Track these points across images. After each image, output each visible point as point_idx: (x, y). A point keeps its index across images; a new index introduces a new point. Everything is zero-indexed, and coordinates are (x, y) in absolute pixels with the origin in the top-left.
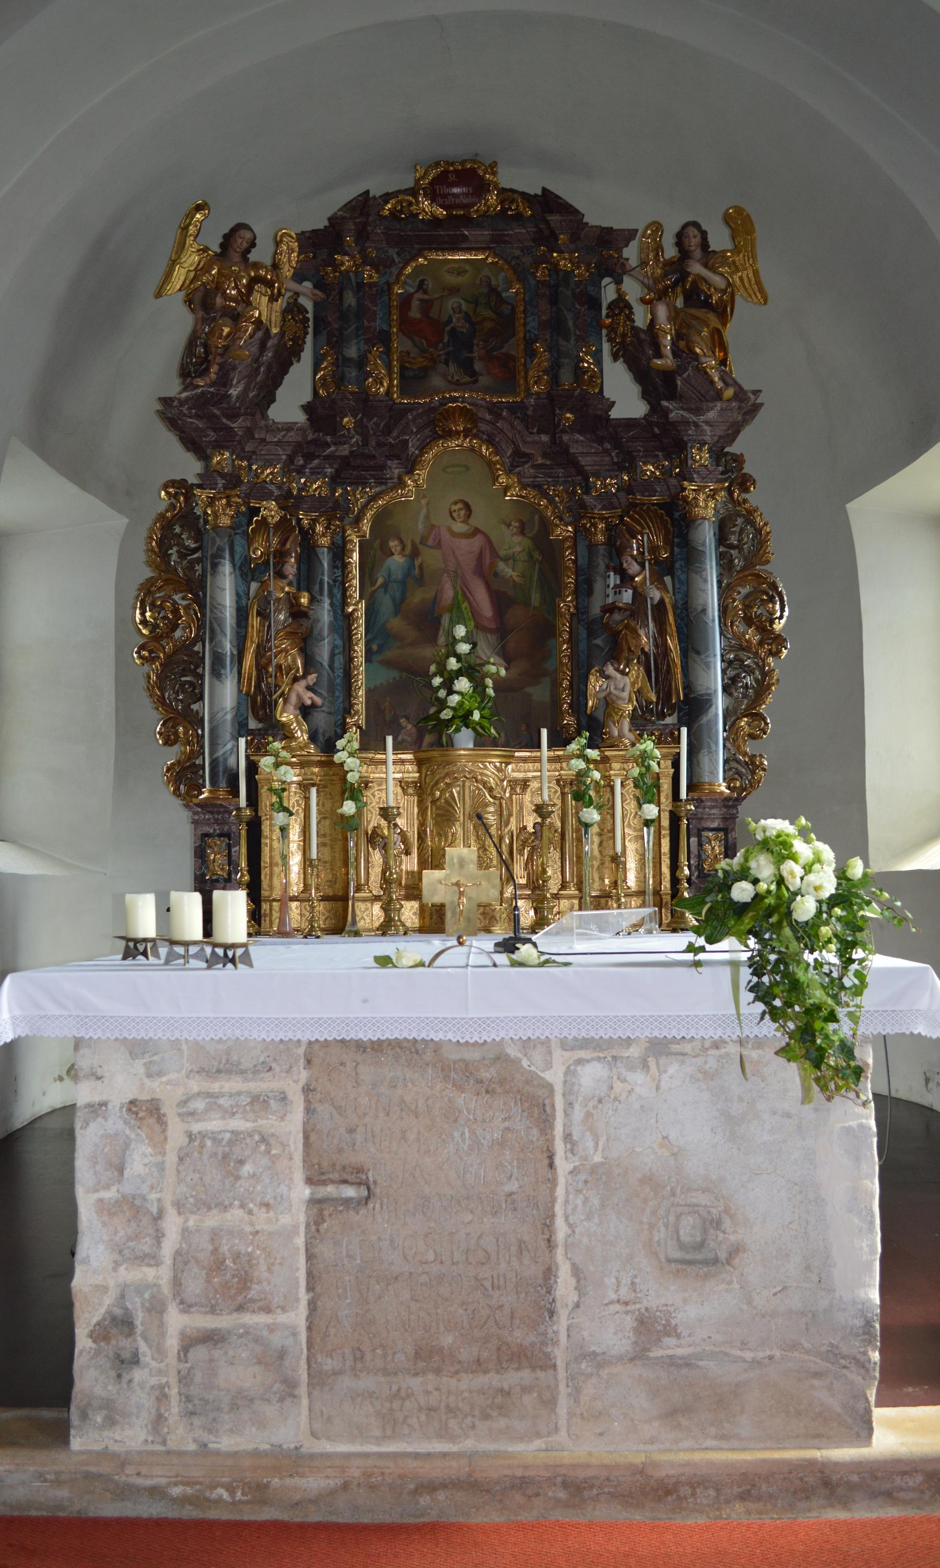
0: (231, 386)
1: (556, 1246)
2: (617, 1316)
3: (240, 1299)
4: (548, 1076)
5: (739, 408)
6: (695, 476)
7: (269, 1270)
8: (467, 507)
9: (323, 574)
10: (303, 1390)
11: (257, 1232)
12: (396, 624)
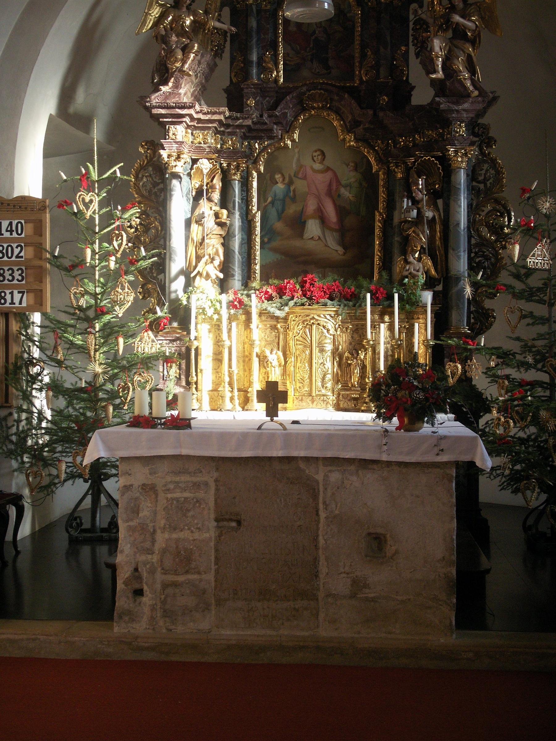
0: (181, 88)
1: (319, 549)
2: (344, 579)
3: (187, 568)
4: (316, 477)
5: (483, 101)
6: (456, 142)
7: (200, 556)
8: (323, 154)
9: (235, 197)
10: (213, 607)
11: (195, 540)
12: (279, 226)
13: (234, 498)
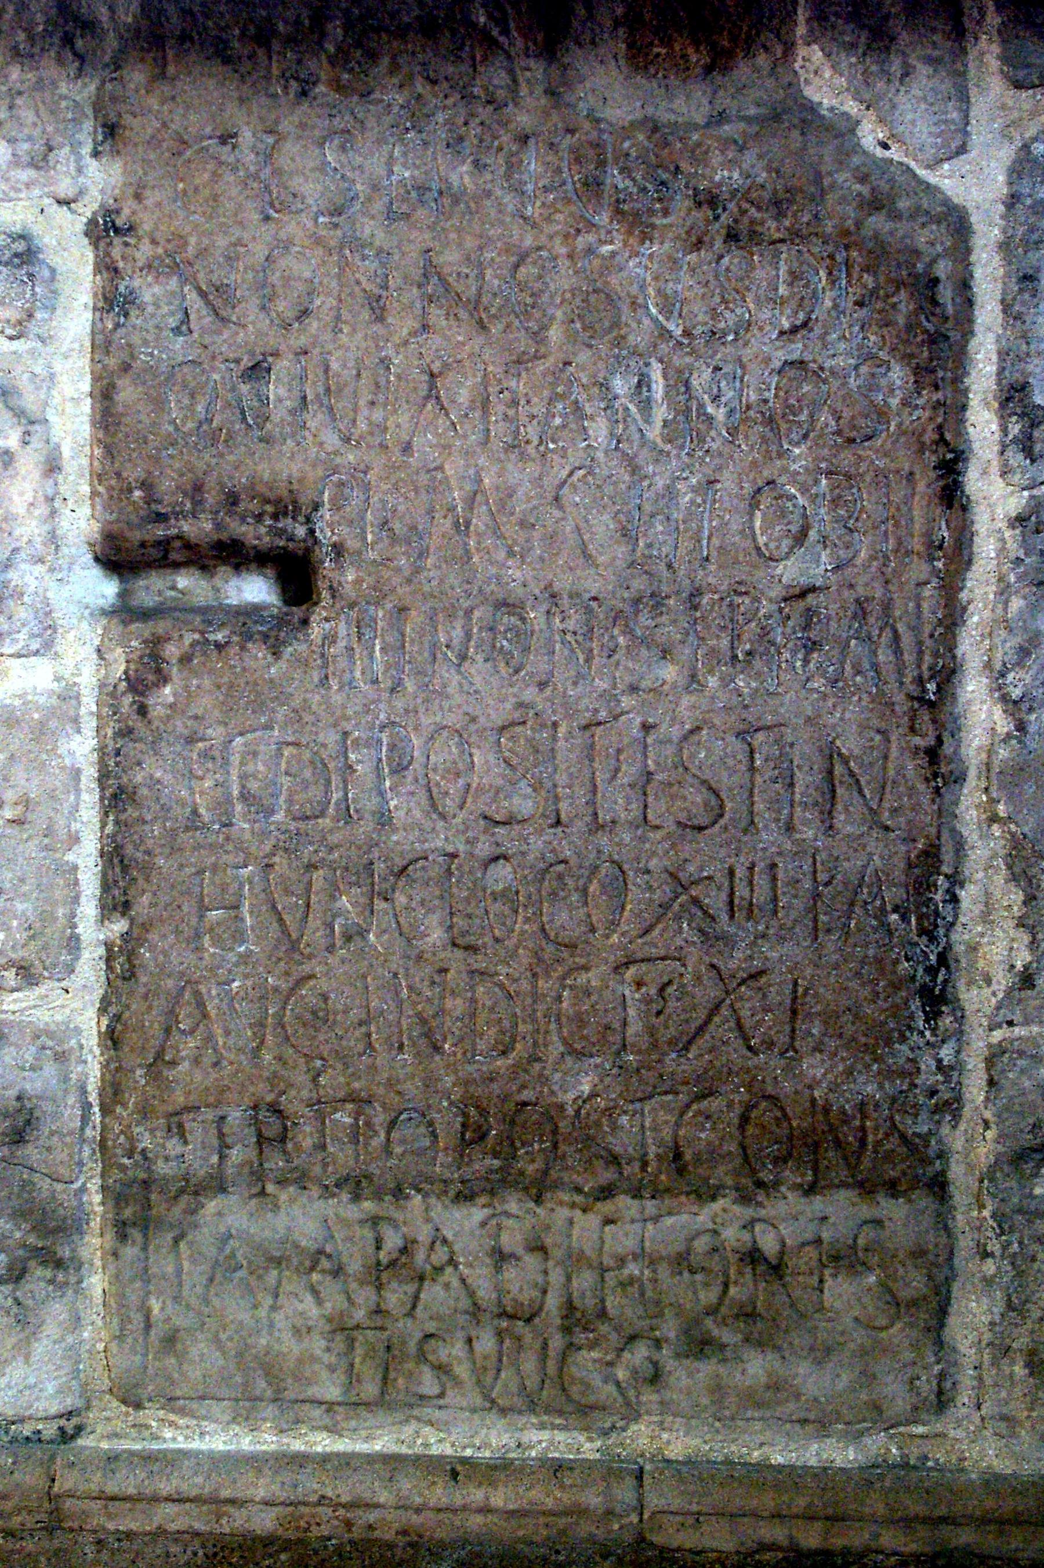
10: (93, 1244)
13: (257, 371)
